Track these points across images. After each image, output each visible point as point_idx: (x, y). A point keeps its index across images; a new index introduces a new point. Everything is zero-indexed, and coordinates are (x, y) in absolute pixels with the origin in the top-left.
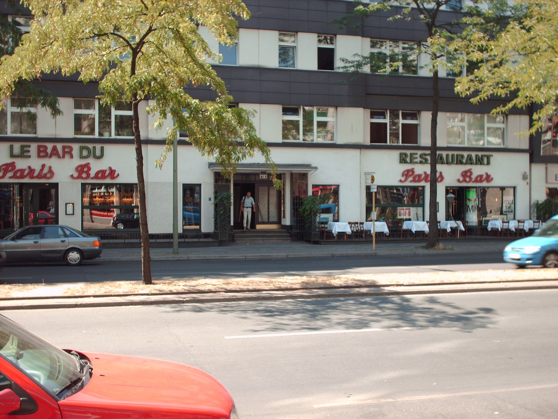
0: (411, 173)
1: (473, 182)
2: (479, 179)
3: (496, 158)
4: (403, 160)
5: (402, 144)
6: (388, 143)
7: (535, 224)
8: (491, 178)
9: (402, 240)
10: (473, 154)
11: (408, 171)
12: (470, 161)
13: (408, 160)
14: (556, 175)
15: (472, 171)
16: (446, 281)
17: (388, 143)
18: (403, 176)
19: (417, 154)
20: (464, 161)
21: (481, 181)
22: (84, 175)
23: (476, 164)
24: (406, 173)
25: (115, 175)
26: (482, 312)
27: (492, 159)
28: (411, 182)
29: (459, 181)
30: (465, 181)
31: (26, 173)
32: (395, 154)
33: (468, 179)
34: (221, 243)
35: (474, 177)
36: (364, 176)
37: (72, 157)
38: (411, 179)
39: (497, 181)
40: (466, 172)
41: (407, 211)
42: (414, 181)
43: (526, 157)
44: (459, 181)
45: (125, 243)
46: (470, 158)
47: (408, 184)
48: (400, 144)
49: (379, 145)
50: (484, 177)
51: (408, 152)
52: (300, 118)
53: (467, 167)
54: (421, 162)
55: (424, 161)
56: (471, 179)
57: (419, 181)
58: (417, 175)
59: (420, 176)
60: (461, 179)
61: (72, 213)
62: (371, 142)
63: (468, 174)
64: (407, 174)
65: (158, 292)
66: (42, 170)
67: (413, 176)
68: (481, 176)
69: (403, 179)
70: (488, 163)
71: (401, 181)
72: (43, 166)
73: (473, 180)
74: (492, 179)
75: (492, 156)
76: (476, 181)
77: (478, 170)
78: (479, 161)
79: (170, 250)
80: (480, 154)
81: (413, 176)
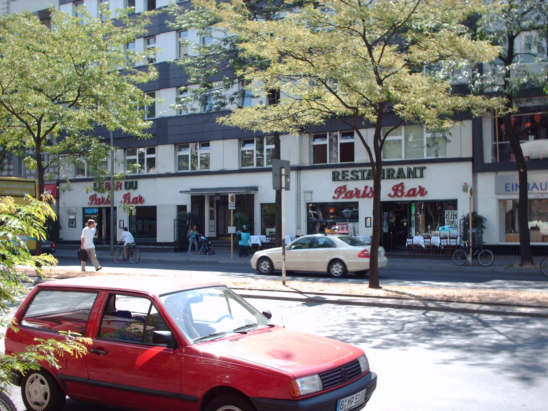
0: (343, 190)
1: (405, 196)
2: (411, 193)
3: (430, 169)
4: (335, 178)
5: (340, 163)
6: (328, 163)
7: (442, 240)
8: (425, 191)
9: (432, 256)
10: (405, 168)
11: (340, 188)
12: (401, 175)
13: (340, 178)
14: (506, 185)
15: (404, 185)
16: (203, 289)
17: (328, 163)
18: (336, 193)
19: (348, 171)
20: (395, 175)
21: (414, 195)
22: (399, 194)
23: (409, 177)
24: (339, 190)
25: (424, 193)
26: (426, 333)
27: (425, 171)
28: (343, 198)
29: (334, 198)
30: (396, 195)
31: (354, 193)
32: (329, 173)
33: (399, 194)
34: (176, 250)
35: (406, 191)
36: (303, 194)
37: (121, 189)
38: (343, 195)
39: (433, 195)
40: (397, 186)
41: (345, 226)
42: (346, 197)
43: (469, 166)
44: (390, 195)
45: (102, 247)
46: (401, 171)
47: (340, 200)
48: (339, 163)
49: (348, 164)
50: (418, 190)
51: (340, 170)
52: (327, 142)
53: (398, 181)
54: (352, 179)
55: (354, 177)
56: (403, 193)
57: (351, 197)
58: (98, 199)
59: (351, 192)
60: (392, 193)
61: (370, 226)
62: (314, 163)
63: (400, 188)
64: (340, 191)
65: (293, 290)
66: (365, 191)
67: (345, 193)
68: (414, 190)
69: (336, 196)
70: (422, 176)
71: (334, 198)
72: (366, 187)
73: (406, 193)
74: (426, 192)
75: (425, 168)
76: (408, 195)
77: (410, 184)
78: (412, 174)
79: (109, 252)
80: (412, 167)
81: (345, 193)
